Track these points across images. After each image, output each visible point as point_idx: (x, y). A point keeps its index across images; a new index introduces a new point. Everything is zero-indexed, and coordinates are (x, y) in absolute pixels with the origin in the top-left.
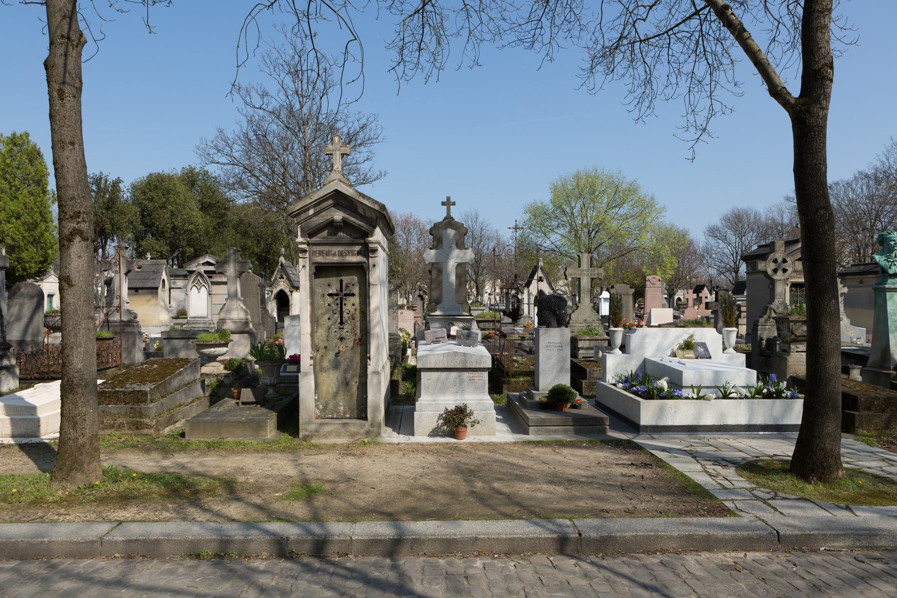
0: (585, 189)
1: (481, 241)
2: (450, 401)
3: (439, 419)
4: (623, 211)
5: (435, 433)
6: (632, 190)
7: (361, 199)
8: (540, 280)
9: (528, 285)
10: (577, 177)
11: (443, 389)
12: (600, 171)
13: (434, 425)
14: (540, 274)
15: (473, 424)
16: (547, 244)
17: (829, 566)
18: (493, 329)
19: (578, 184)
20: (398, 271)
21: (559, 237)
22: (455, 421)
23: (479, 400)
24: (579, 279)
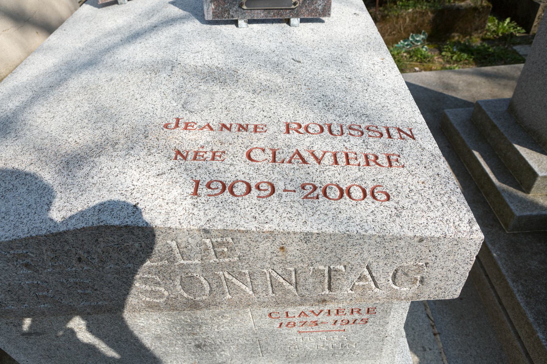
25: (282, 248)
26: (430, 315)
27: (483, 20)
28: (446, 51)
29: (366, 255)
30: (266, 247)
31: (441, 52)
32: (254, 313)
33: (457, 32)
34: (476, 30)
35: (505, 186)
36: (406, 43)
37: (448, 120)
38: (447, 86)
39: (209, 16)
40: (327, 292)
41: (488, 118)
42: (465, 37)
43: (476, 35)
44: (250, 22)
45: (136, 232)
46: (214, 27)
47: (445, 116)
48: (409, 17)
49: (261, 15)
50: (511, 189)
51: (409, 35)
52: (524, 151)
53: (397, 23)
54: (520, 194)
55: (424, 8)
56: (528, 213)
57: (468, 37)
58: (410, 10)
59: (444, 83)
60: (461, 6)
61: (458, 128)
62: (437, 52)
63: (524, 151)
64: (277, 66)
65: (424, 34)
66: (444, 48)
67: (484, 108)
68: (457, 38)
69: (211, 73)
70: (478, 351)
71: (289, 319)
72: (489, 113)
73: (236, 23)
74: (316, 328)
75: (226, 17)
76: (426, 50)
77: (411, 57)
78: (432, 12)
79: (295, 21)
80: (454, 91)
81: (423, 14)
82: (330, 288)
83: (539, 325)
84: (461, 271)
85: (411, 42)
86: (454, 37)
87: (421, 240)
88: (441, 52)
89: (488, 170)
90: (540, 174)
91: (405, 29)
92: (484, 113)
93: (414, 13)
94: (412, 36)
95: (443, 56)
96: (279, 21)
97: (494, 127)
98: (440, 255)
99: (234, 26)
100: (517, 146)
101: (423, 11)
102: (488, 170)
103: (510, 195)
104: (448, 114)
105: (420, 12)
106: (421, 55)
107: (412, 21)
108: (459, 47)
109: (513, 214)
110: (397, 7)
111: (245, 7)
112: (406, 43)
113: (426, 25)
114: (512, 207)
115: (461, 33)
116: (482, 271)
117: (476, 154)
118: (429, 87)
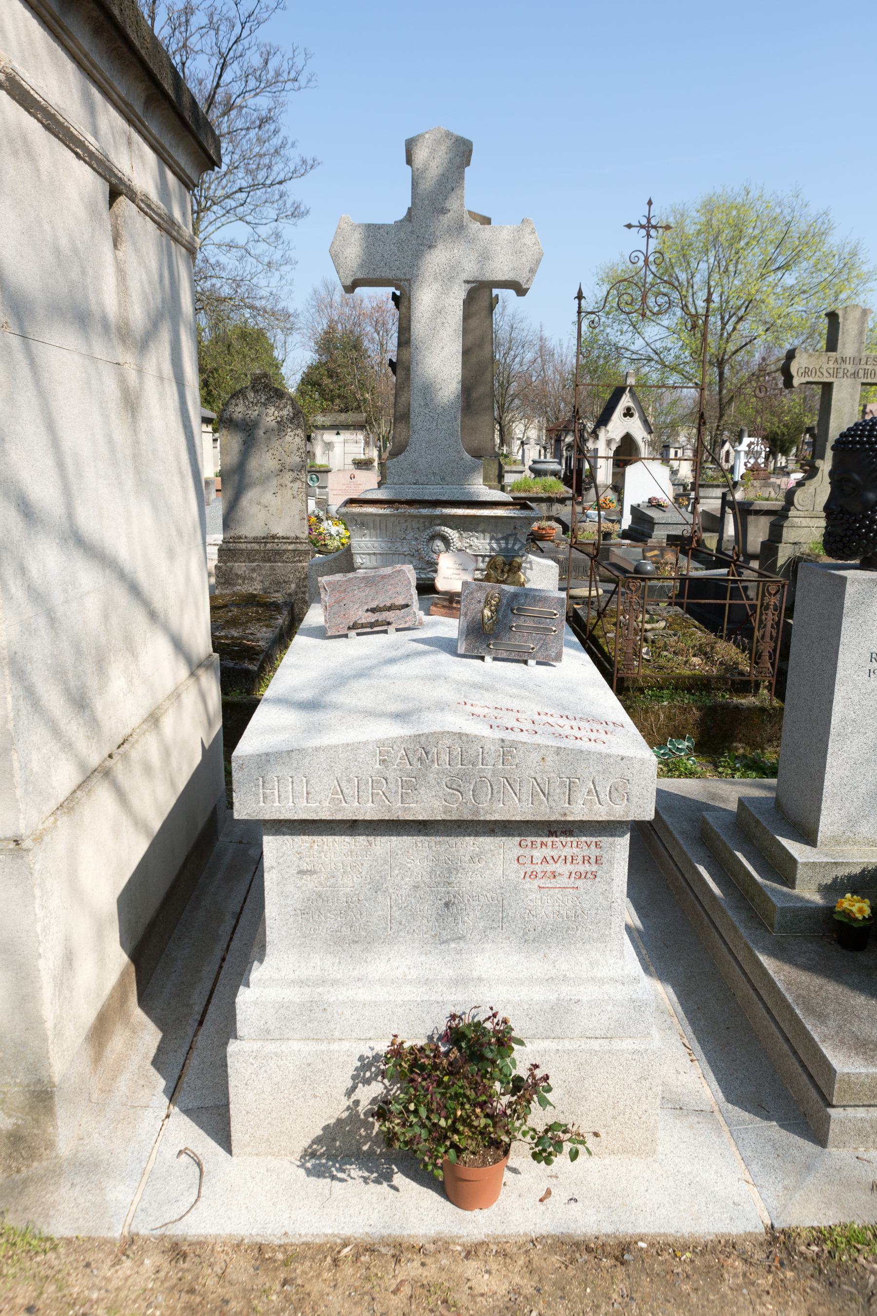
0: (726, 232)
1: (510, 349)
2: (403, 995)
3: (360, 1078)
4: (789, 279)
5: (334, 1151)
6: (814, 237)
7: (32, 92)
8: (628, 413)
9: (604, 420)
10: (709, 207)
11: (351, 930)
12: (754, 193)
13: (334, 1109)
14: (626, 401)
15: (546, 1147)
16: (639, 344)
17: (146, 209)
18: (646, 631)
19: (709, 223)
20: (365, 400)
21: (664, 333)
22: (449, 1102)
23: (585, 995)
24: (827, 388)
25: (543, 759)
26: (687, 1044)
27: (777, 727)
28: (724, 767)
29: (591, 769)
30: (535, 756)
31: (716, 767)
32: (506, 856)
33: (740, 741)
34: (770, 740)
35: (768, 883)
36: (662, 751)
37: (707, 823)
38: (714, 796)
39: (461, 650)
40: (567, 805)
41: (751, 814)
42: (753, 750)
43: (770, 749)
44: (495, 659)
45: (464, 738)
46: (464, 660)
47: (705, 821)
48: (664, 713)
49: (504, 655)
50: (775, 885)
51: (666, 739)
52: (786, 843)
53: (646, 720)
54: (785, 889)
55: (686, 701)
56: (791, 904)
57: (759, 751)
58: (665, 703)
59: (709, 793)
60: (742, 705)
61: (718, 830)
62: (711, 767)
63: (786, 843)
64: (522, 687)
65: (689, 740)
66: (720, 762)
67: (746, 803)
68: (741, 751)
69: (442, 709)
70: (746, 1074)
71: (534, 866)
72: (752, 809)
73: (482, 658)
74: (553, 883)
75: (475, 653)
76: (695, 763)
77: (670, 771)
78: (698, 708)
79: (532, 662)
80: (724, 802)
81: (684, 710)
82: (569, 803)
83: (798, 1004)
84: (650, 790)
85: (670, 750)
86: (736, 749)
87: (622, 759)
88: (716, 767)
89: (750, 868)
90: (799, 860)
91: (659, 729)
92: (747, 810)
93: (670, 708)
94: (671, 741)
95: (720, 773)
96: (518, 661)
97: (757, 821)
98: (635, 772)
99: (479, 662)
100: (778, 837)
101: (685, 706)
102: (750, 868)
103: (773, 890)
104: (707, 817)
105: (680, 708)
106: (686, 769)
107: (670, 718)
108: (744, 762)
109: (774, 906)
110: (644, 697)
111: (491, 647)
112: (662, 751)
113: (690, 726)
114: (773, 899)
115: (748, 744)
116: (748, 986)
117: (739, 854)
118: (688, 796)
